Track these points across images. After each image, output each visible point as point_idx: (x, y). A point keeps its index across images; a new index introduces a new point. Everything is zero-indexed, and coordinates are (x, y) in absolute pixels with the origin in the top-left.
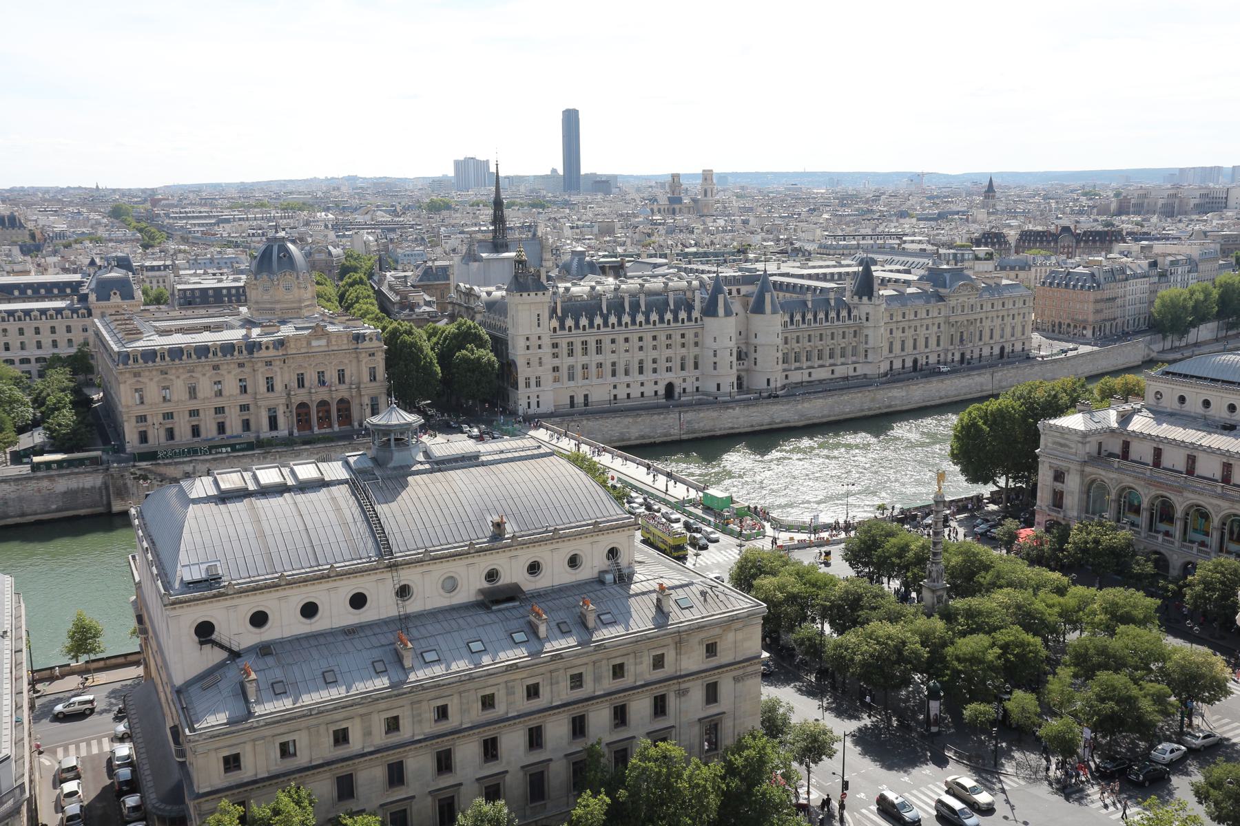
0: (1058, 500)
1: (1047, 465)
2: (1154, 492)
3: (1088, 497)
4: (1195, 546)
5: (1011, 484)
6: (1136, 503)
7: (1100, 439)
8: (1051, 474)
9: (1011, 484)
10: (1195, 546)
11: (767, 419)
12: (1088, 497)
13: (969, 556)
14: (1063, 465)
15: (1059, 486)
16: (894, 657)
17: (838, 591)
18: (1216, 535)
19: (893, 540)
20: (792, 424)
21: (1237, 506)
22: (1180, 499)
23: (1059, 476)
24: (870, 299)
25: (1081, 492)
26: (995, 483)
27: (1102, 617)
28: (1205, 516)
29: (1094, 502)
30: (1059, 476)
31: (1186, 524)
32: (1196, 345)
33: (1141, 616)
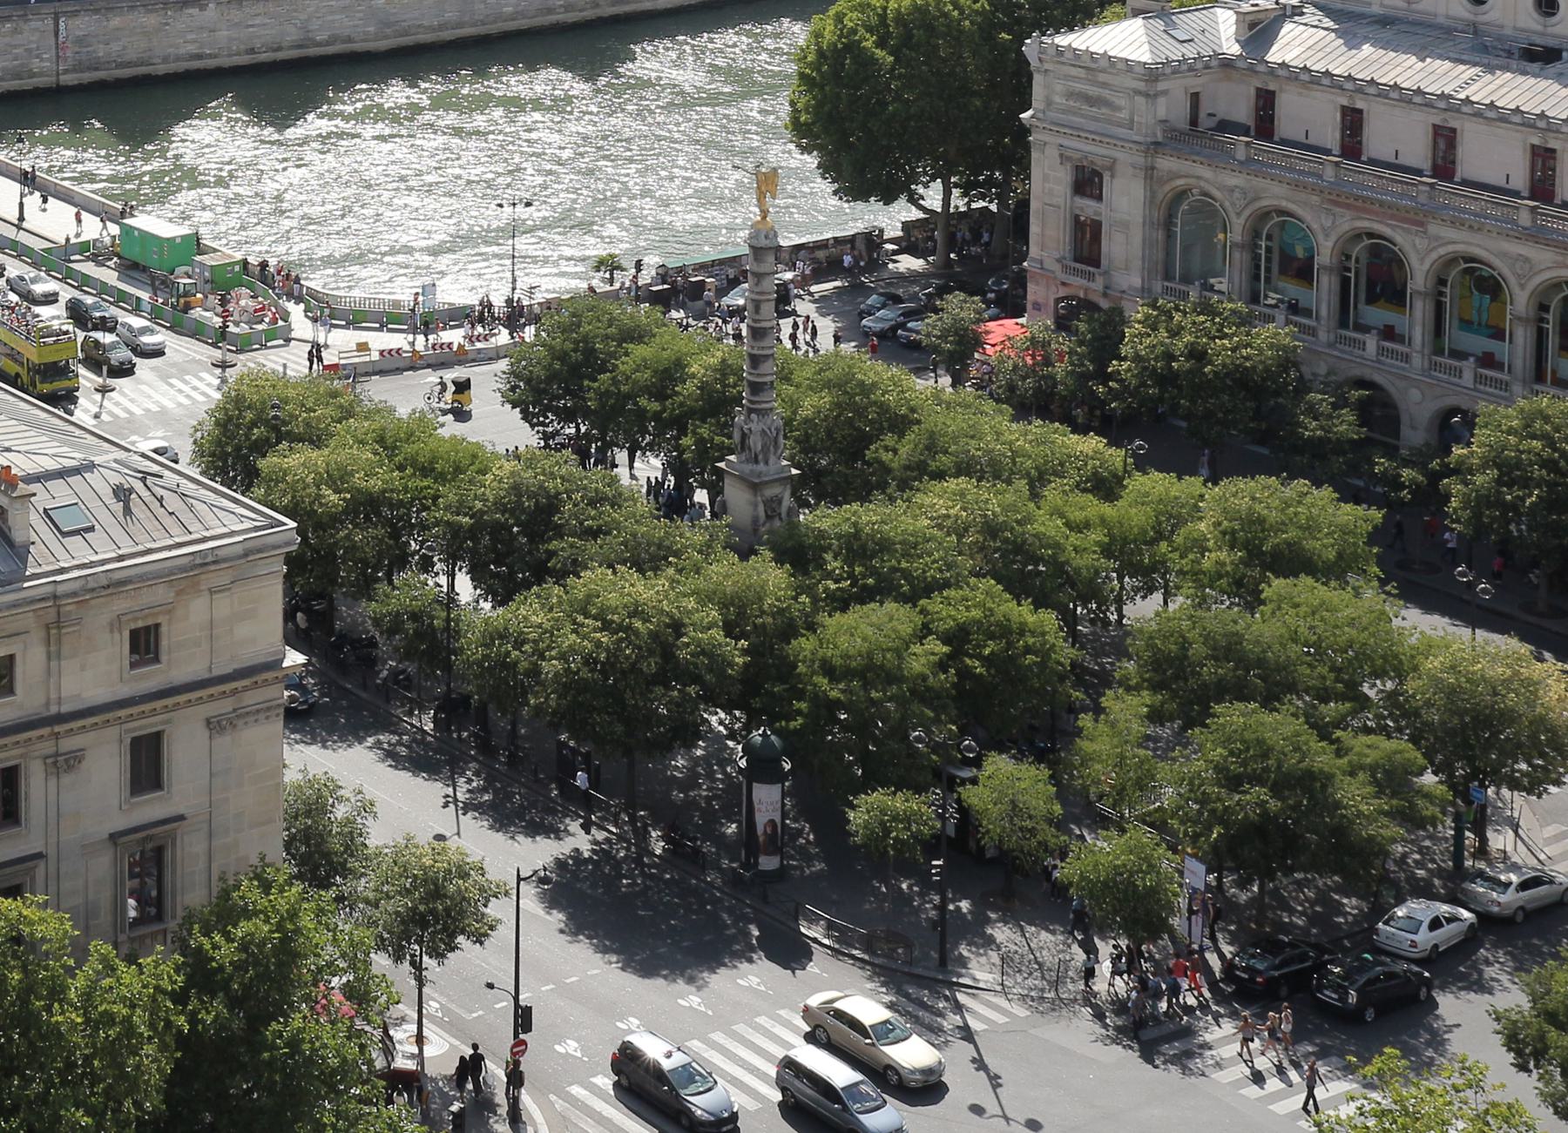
0: (1086, 244)
1: (1052, 153)
2: (1347, 223)
3: (1170, 236)
4: (1468, 367)
6: (1300, 252)
7: (1195, 83)
10: (1468, 367)
11: (292, 34)
12: (1170, 236)
15: (1088, 207)
17: (491, 487)
18: (1522, 338)
20: (358, 47)
23: (1087, 182)
26: (914, 200)
27: (1223, 555)
29: (1186, 249)
30: (1087, 182)
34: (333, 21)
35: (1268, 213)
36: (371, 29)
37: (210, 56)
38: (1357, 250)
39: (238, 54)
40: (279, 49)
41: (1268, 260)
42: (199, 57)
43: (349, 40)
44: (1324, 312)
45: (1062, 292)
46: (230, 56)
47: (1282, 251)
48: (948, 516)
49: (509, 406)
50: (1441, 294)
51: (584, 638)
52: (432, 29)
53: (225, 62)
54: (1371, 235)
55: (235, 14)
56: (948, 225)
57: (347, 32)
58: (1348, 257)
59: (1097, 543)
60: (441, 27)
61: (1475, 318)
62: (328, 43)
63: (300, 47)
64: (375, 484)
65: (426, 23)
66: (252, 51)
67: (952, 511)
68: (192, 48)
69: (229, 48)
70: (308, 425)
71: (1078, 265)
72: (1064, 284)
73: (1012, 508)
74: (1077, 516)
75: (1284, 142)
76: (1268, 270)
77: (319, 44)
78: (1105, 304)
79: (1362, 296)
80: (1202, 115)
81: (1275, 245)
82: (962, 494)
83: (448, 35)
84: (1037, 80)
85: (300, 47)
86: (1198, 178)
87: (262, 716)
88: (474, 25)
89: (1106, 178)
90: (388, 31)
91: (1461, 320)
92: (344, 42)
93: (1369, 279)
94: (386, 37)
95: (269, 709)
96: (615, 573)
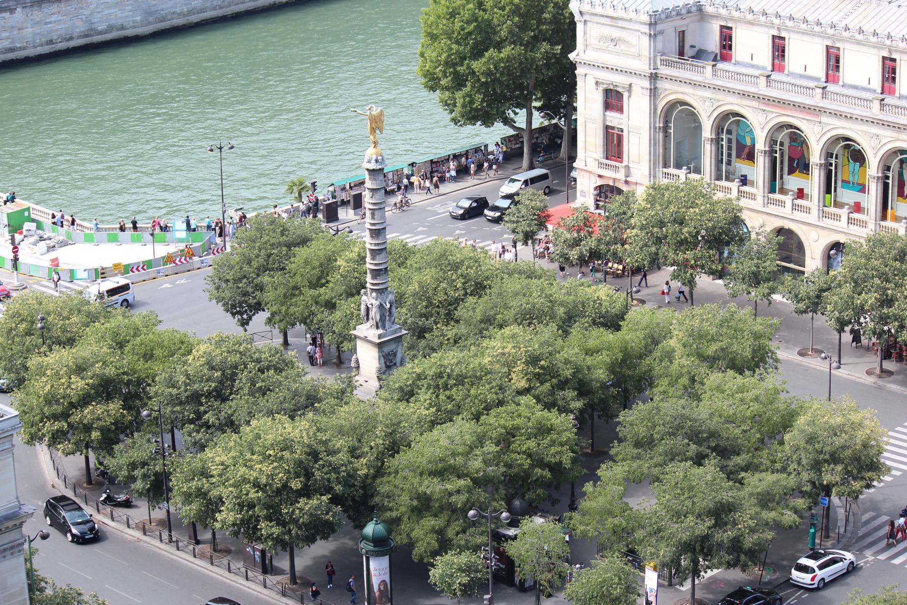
0: (613, 144)
1: (591, 81)
2: (777, 117)
3: (666, 136)
4: (844, 212)
5: (538, 120)
6: (749, 143)
7: (680, 24)
8: (598, 98)
9: (538, 120)
10: (844, 212)
11: (80, 27)
12: (666, 136)
13: (445, 262)
14: (619, 80)
15: (614, 119)
16: (296, 484)
17: (195, 362)
18: (874, 189)
19: (302, 253)
20: (129, 33)
21: (903, 136)
22: (817, 129)
23: (613, 99)
24: (381, 132)
25: (653, 128)
26: (507, 122)
27: (684, 361)
28: (858, 157)
29: (678, 145)
30: (613, 99)
31: (886, 187)
32: (401, 46)
33: (748, 354)
34: (109, 14)
35: (728, 115)
36: (138, 18)
37: (21, 49)
38: (782, 136)
39: (41, 45)
40: (71, 39)
41: (730, 148)
42: (12, 50)
43: (123, 28)
44: (761, 183)
45: (600, 182)
46: (35, 47)
47: (738, 141)
48: (504, 354)
49: (214, 301)
50: (887, 178)
51: (251, 468)
52: (183, 15)
53: (31, 52)
54: (791, 126)
55: (37, 14)
56: (531, 138)
57: (120, 22)
58: (775, 142)
59: (605, 363)
60: (190, 13)
61: (851, 180)
62: (106, 32)
63: (86, 36)
64: (110, 371)
65: (178, 10)
66: (51, 42)
67: (506, 350)
68: (6, 44)
69: (34, 42)
70: (64, 330)
71: (608, 162)
72: (600, 176)
73: (546, 343)
74: (592, 343)
75: (790, 74)
76: (729, 155)
77: (101, 33)
78: (625, 188)
79: (786, 169)
80: (687, 47)
81: (733, 137)
82: (513, 336)
83: (195, 18)
84: (580, 28)
85: (86, 36)
86: (683, 93)
87: (8, 553)
88: (214, 9)
89: (626, 95)
90: (151, 19)
91: (843, 181)
92: (118, 30)
93: (789, 157)
94: (150, 23)
95: (12, 548)
96: (274, 419)
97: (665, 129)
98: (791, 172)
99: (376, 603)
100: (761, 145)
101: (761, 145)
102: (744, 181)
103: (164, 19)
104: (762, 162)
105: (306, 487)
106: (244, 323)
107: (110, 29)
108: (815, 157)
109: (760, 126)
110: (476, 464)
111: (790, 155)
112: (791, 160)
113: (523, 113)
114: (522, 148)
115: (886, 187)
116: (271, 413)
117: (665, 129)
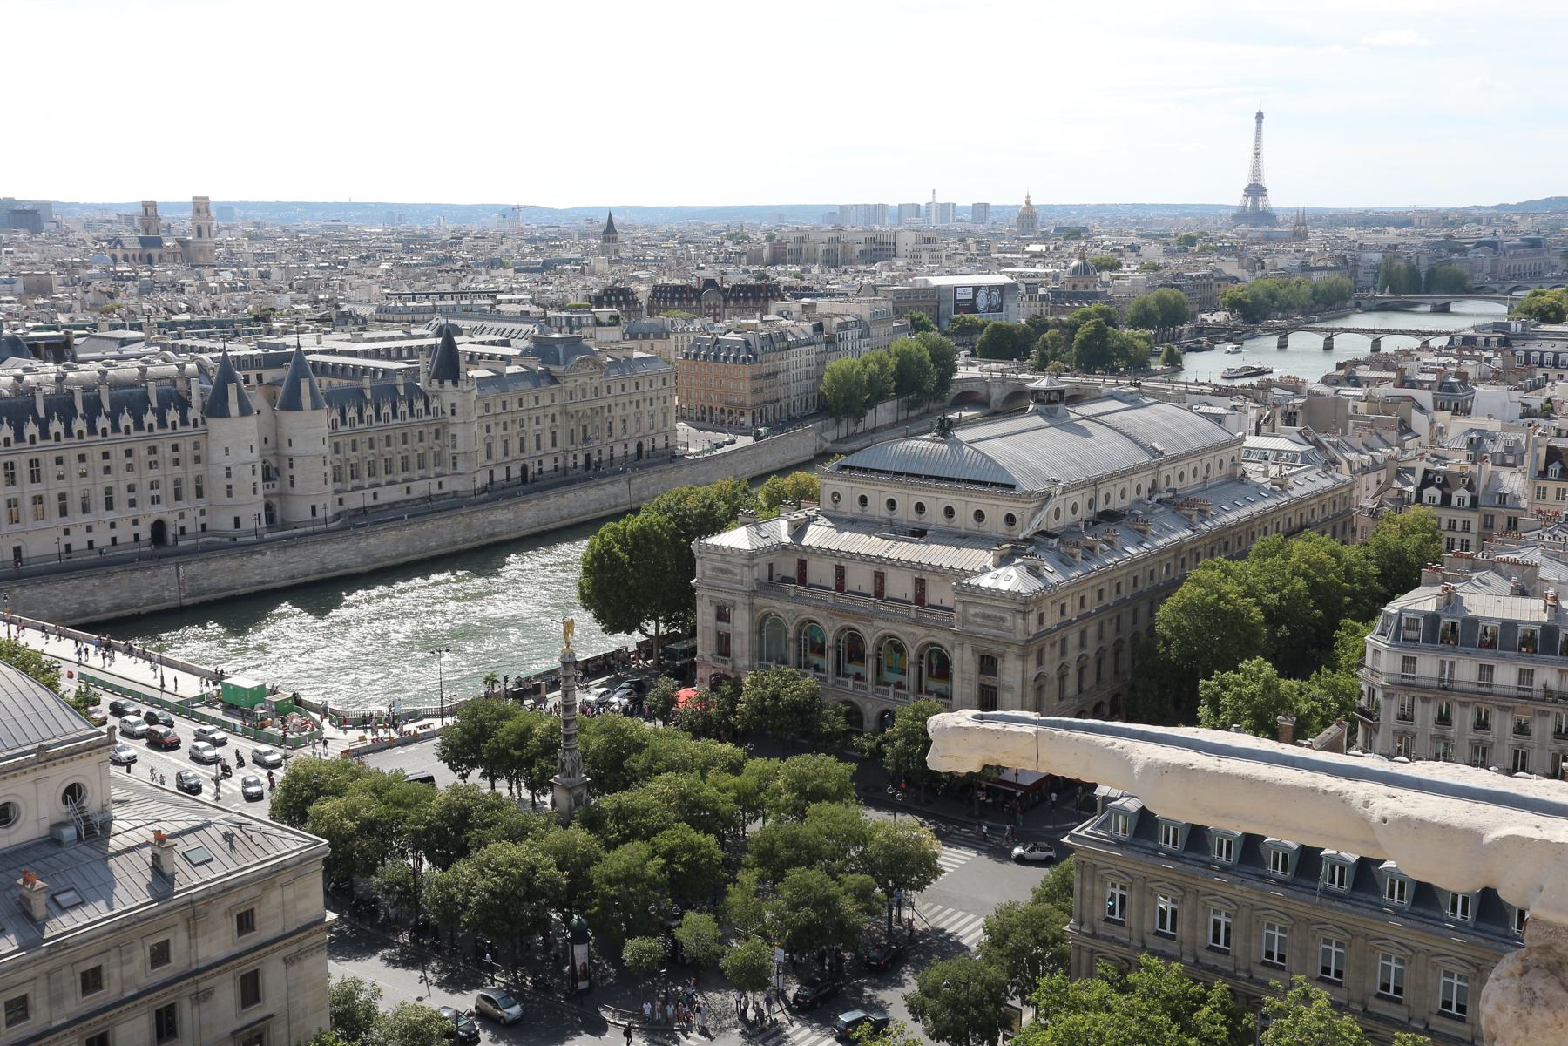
0: (723, 645)
1: (706, 599)
2: (840, 623)
3: (761, 637)
4: (891, 689)
7: (770, 559)
9: (663, 630)
10: (891, 689)
11: (315, 566)
12: (761, 637)
18: (913, 672)
19: (509, 724)
23: (722, 616)
27: (788, 796)
29: (769, 644)
30: (722, 616)
31: (920, 670)
33: (835, 789)
42: (263, 583)
43: (347, 567)
52: (392, 558)
60: (397, 556)
66: (293, 577)
74: (723, 785)
83: (401, 561)
84: (698, 562)
97: (760, 631)
98: (850, 661)
99: (27, 920)
100: (830, 642)
101: (830, 642)
102: (858, 677)
103: (378, 561)
104: (871, 663)
105: (527, 893)
106: (463, 777)
107: (338, 567)
108: (870, 649)
109: (830, 630)
110: (651, 872)
111: (853, 648)
112: (850, 653)
113: (653, 624)
114: (1275, 735)
115: (920, 670)
116: (498, 840)
117: (760, 631)
